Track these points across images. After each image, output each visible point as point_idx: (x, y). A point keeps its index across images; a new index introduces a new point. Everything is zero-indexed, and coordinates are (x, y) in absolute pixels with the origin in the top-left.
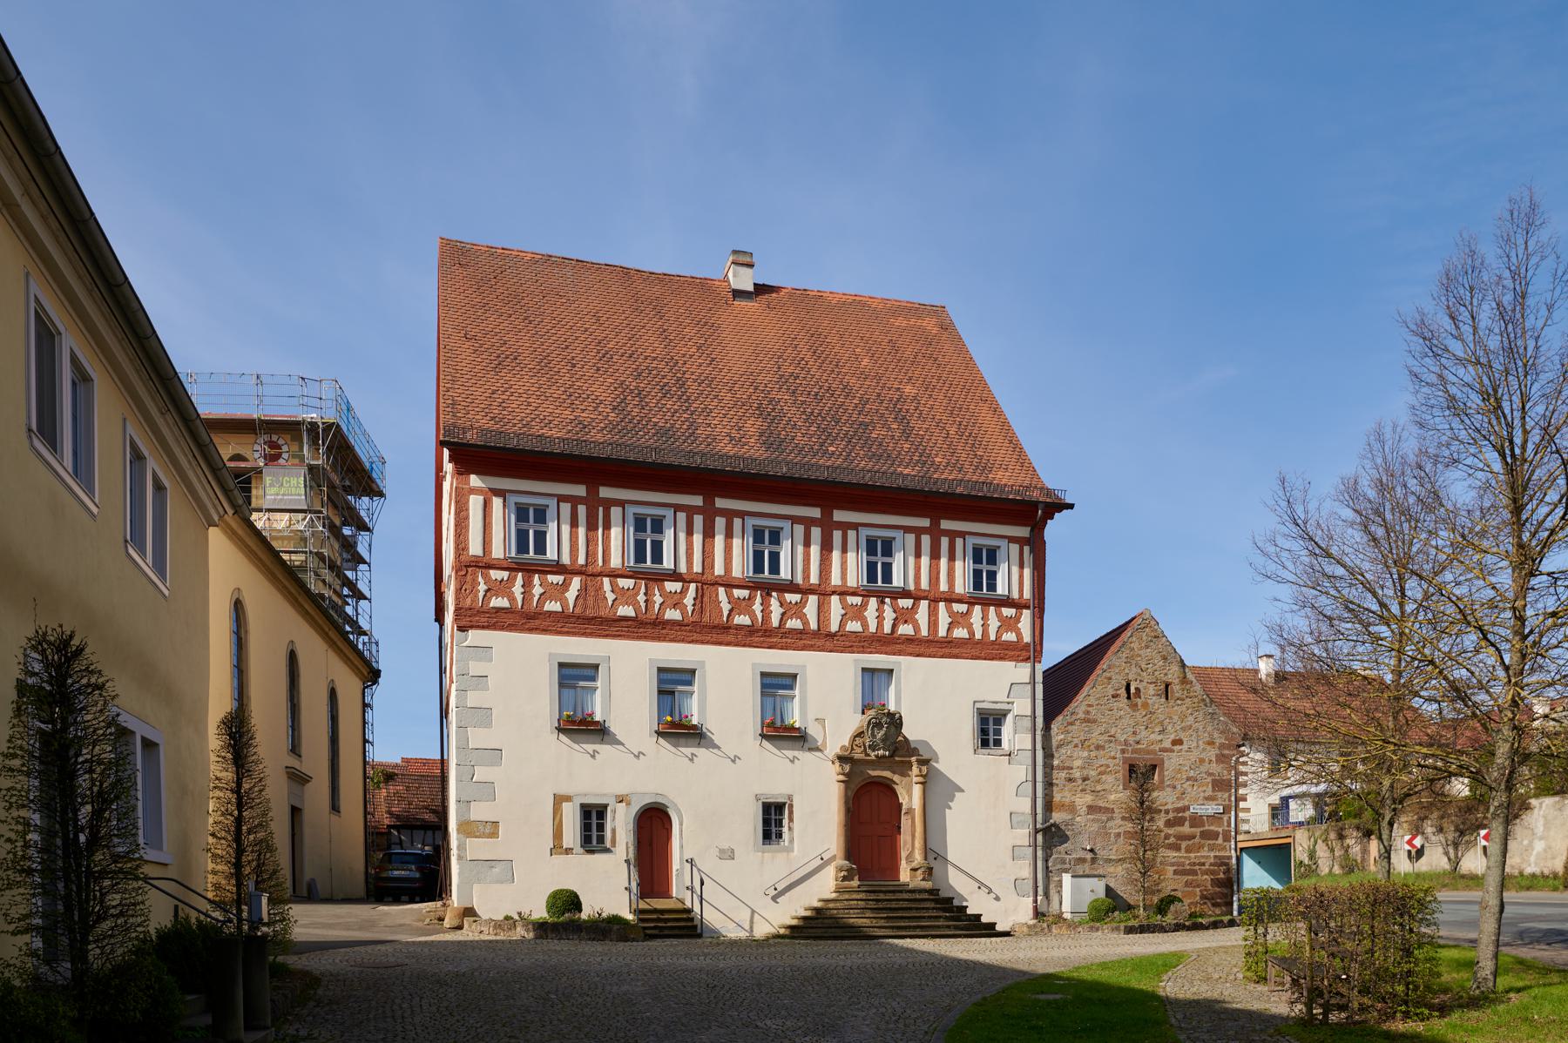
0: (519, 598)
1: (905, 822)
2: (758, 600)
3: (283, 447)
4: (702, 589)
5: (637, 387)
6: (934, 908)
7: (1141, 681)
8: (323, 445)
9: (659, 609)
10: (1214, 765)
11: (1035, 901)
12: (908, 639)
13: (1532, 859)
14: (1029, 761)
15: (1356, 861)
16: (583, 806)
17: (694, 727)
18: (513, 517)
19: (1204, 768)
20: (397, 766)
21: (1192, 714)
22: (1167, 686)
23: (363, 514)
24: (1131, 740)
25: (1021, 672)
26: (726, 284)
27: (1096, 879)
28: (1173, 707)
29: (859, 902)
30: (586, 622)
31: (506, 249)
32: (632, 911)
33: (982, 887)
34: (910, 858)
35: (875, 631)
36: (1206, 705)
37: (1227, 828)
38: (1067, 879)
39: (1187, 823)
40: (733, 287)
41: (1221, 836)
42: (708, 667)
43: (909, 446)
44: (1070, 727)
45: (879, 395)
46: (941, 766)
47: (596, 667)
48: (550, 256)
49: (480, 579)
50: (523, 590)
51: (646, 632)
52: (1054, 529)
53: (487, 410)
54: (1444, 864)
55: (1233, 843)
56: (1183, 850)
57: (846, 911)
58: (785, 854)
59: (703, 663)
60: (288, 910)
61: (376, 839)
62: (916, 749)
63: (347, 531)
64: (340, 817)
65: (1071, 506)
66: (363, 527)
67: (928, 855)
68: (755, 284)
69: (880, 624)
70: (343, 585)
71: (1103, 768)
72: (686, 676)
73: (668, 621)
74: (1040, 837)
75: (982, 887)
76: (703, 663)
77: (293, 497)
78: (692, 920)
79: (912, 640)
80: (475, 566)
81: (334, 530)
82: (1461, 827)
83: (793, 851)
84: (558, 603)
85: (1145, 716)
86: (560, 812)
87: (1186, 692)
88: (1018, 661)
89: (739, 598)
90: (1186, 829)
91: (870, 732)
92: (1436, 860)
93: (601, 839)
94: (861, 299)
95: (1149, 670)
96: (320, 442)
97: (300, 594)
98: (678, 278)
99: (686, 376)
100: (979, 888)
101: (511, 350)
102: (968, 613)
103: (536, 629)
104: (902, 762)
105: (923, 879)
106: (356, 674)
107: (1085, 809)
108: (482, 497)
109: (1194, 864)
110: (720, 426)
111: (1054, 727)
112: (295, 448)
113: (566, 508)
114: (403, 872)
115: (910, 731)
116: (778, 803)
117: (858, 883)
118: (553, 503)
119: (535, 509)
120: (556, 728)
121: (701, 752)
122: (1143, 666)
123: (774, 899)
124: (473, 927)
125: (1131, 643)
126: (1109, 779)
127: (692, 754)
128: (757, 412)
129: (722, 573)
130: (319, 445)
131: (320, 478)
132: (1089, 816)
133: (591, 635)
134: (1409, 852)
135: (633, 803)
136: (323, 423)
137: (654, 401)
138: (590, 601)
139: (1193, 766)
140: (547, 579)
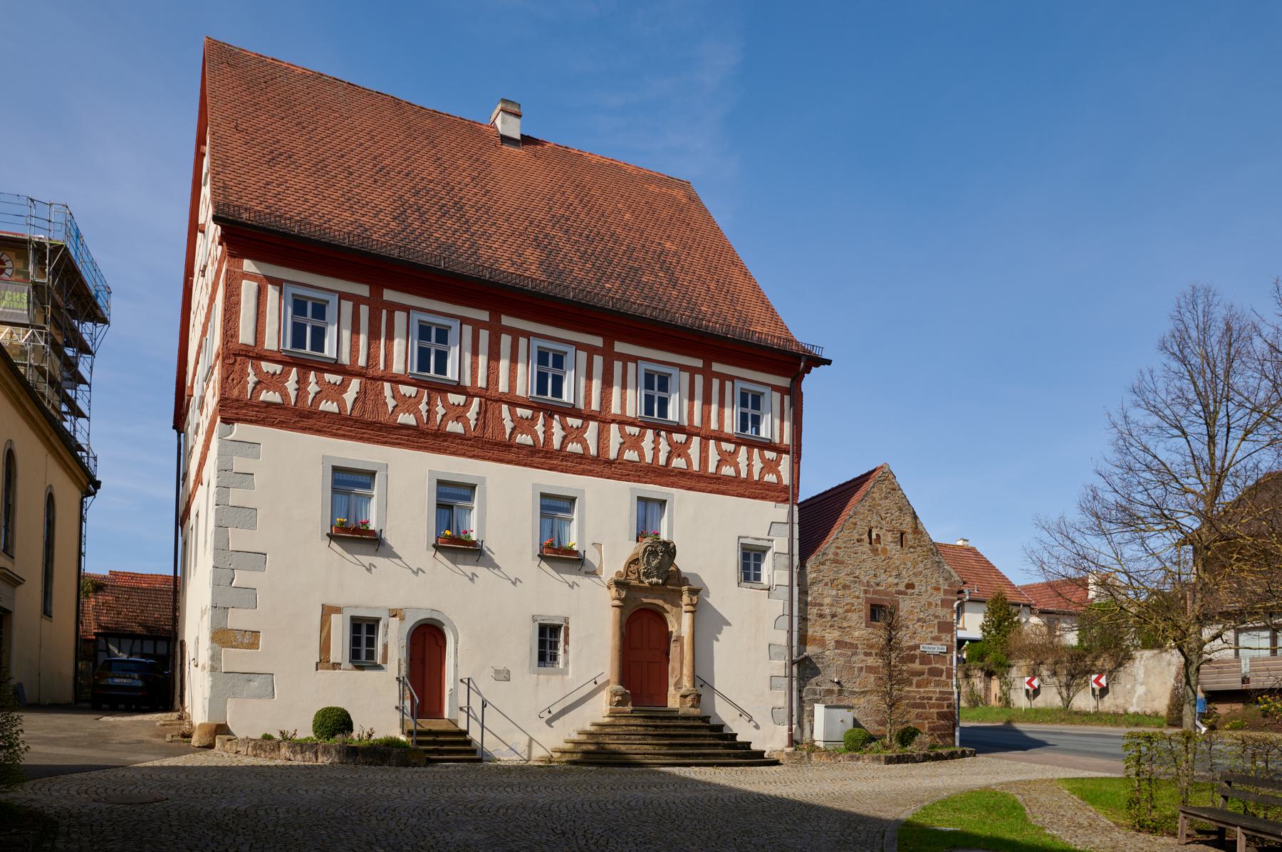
0: (293, 395)
1: (674, 650)
2: (541, 421)
3: (6, 263)
4: (486, 405)
5: (416, 203)
6: (711, 736)
7: (881, 528)
8: (50, 265)
9: (442, 420)
10: (940, 608)
11: (791, 730)
12: (680, 472)
13: (1134, 700)
14: (787, 596)
15: (980, 696)
16: (353, 619)
17: (474, 543)
18: (290, 310)
19: (931, 611)
20: (105, 577)
21: (922, 562)
22: (902, 534)
23: (86, 337)
24: (873, 581)
25: (780, 512)
26: (494, 130)
27: (846, 710)
28: (907, 554)
29: (639, 728)
30: (362, 426)
31: (276, 60)
32: (405, 732)
33: (743, 716)
34: (678, 685)
35: (651, 462)
36: (933, 554)
37: (948, 666)
38: (819, 710)
39: (917, 661)
40: (501, 133)
41: (944, 673)
42: (488, 483)
43: (677, 294)
44: (821, 567)
45: (643, 246)
46: (711, 600)
47: (373, 474)
48: (322, 75)
49: (250, 370)
50: (297, 387)
51: (426, 442)
52: (812, 382)
53: (262, 199)
54: (1057, 702)
55: (954, 680)
56: (914, 685)
57: (627, 737)
58: (560, 677)
59: (483, 479)
60: (17, 733)
61: (86, 649)
62: (685, 578)
63: (69, 352)
64: (51, 621)
65: (828, 362)
66: (85, 349)
67: (696, 683)
68: (521, 135)
69: (655, 456)
70: (63, 401)
71: (849, 607)
72: (467, 490)
73: (450, 434)
74: (795, 668)
75: (743, 716)
76: (483, 479)
77: (14, 311)
78: (469, 742)
79: (684, 473)
80: (245, 356)
81: (57, 349)
82: (1073, 671)
83: (567, 674)
84: (335, 403)
85: (884, 560)
86: (328, 624)
87: (917, 541)
88: (777, 502)
89: (522, 417)
90: (916, 666)
91: (645, 559)
92: (1051, 697)
93: (371, 655)
94: (617, 163)
95: (888, 519)
96: (47, 261)
97: (22, 393)
98: (448, 117)
99: (463, 201)
100: (741, 715)
101: (285, 149)
102: (736, 452)
103: (310, 429)
104: (673, 590)
105: (692, 707)
106: (75, 484)
107: (833, 643)
108: (256, 284)
109: (923, 698)
110: (500, 250)
111: (809, 565)
112: (20, 265)
113: (347, 306)
114: (125, 680)
115: (684, 563)
116: (554, 625)
117: (632, 708)
118: (333, 300)
119: (313, 303)
120: (328, 535)
121: (481, 571)
122: (883, 515)
123: (549, 722)
124: (228, 746)
125: (873, 493)
126: (854, 617)
127: (473, 574)
128: (534, 243)
129: (506, 390)
130: (46, 265)
131: (44, 297)
132: (836, 651)
133: (369, 440)
134: (1027, 691)
135: (407, 618)
136: (51, 244)
137: (434, 218)
138: (370, 406)
139: (922, 609)
140: (324, 377)
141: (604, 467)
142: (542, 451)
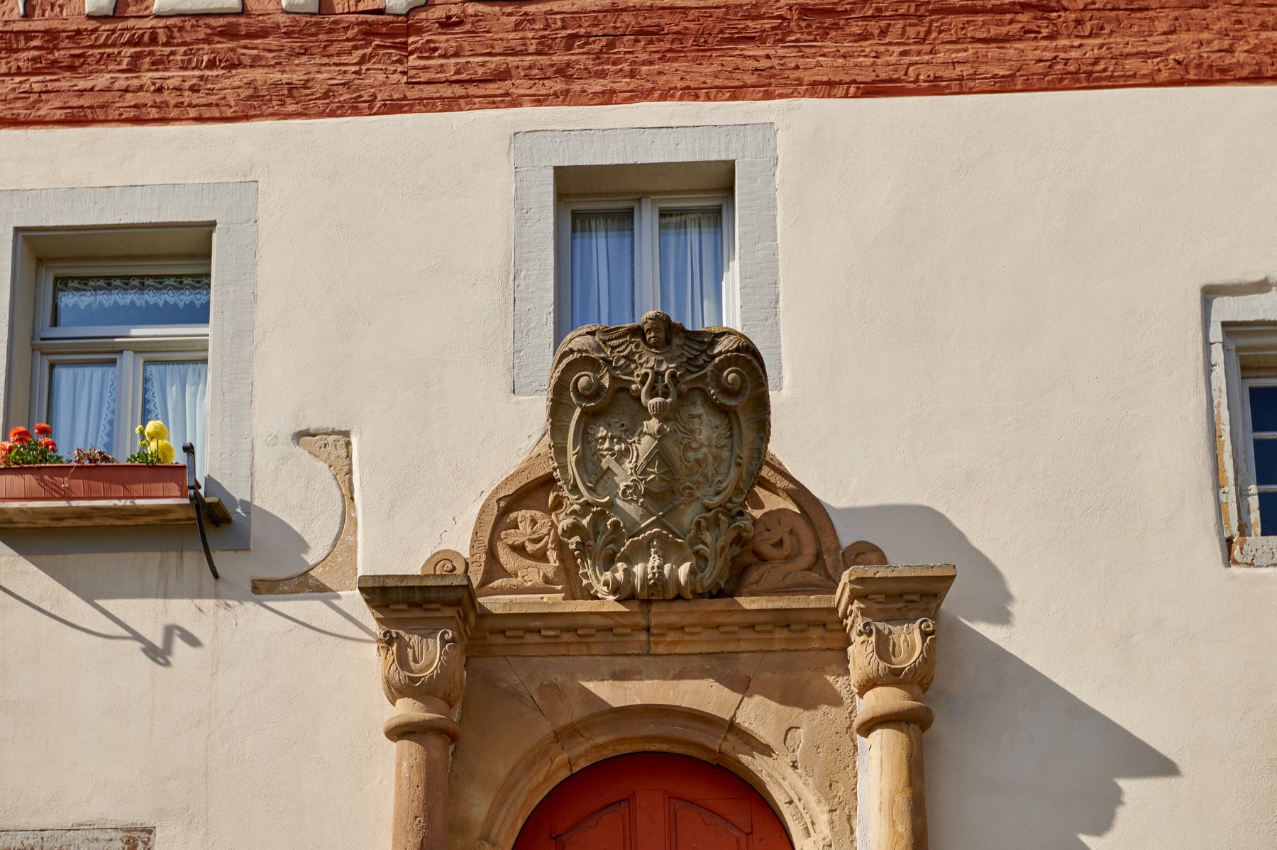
104: (783, 620)
141: (362, 61)
142: (28, 35)
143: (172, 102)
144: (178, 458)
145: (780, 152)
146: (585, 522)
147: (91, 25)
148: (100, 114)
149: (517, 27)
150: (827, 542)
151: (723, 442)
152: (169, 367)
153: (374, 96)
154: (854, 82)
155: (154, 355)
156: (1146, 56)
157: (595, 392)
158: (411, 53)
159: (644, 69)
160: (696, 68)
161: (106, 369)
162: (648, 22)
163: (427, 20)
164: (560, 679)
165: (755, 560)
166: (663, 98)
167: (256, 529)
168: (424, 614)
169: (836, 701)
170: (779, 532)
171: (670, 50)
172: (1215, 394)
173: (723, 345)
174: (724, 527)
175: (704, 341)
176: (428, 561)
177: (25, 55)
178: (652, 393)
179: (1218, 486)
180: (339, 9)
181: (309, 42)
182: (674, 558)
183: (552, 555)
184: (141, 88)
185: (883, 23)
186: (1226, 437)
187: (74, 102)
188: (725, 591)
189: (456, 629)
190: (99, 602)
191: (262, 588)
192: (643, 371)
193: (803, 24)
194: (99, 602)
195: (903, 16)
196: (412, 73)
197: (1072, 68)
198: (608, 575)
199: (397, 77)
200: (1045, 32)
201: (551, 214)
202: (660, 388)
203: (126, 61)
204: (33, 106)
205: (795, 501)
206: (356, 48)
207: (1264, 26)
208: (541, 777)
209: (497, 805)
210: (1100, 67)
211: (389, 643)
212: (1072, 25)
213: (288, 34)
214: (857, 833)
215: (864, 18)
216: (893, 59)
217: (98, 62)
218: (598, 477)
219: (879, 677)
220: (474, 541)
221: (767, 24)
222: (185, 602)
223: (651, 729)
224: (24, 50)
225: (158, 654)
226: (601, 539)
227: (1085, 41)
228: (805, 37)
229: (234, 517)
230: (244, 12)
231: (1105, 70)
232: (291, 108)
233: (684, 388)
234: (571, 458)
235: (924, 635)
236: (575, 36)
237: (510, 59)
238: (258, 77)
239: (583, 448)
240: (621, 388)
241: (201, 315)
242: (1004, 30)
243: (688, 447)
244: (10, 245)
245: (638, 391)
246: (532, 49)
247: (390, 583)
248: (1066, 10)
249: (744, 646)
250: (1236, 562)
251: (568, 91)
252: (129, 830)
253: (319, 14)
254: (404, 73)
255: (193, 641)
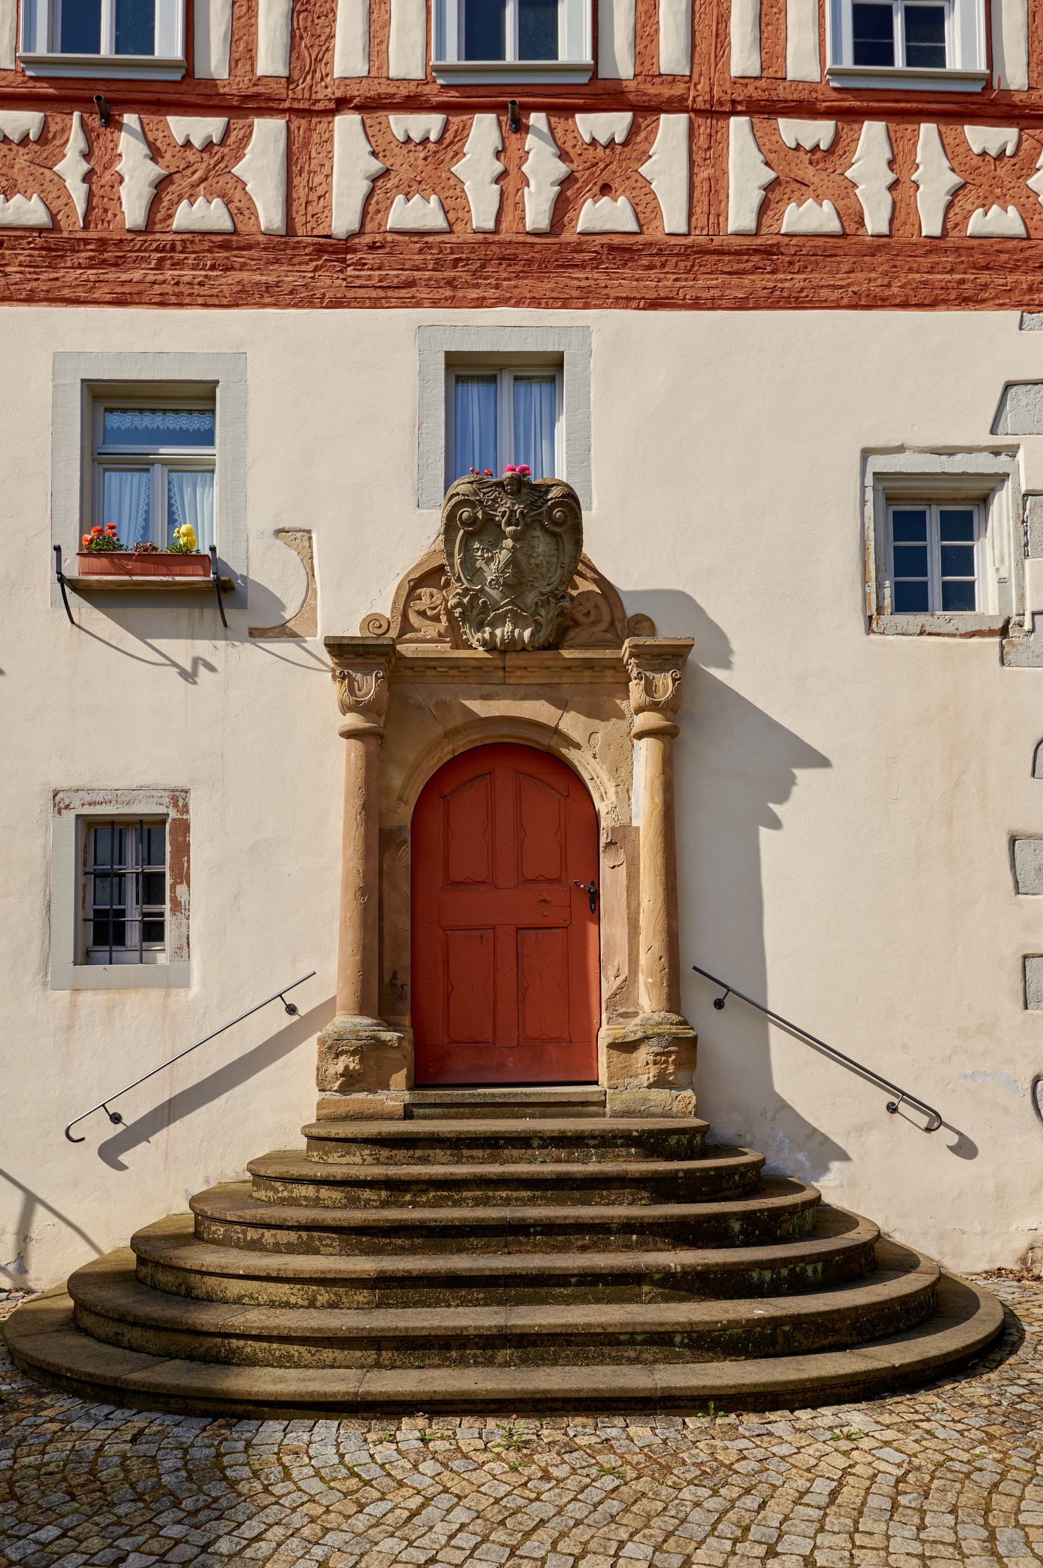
104: (589, 664)
141: (316, 269)
142: (86, 241)
143: (186, 293)
144: (208, 552)
145: (593, 347)
146: (465, 600)
147: (130, 236)
148: (137, 299)
149: (420, 251)
150: (618, 614)
151: (553, 553)
152: (185, 474)
153: (324, 295)
154: (643, 298)
155: (174, 466)
156: (834, 287)
157: (473, 521)
158: (349, 265)
159: (505, 283)
160: (539, 284)
161: (141, 474)
162: (508, 252)
163: (360, 244)
164: (448, 698)
165: (572, 623)
166: (517, 305)
167: (251, 595)
168: (364, 661)
169: (621, 716)
170: (589, 606)
171: (522, 272)
172: (866, 520)
173: (554, 493)
174: (553, 606)
175: (543, 489)
176: (364, 620)
177: (83, 255)
178: (509, 523)
179: (865, 581)
180: (300, 232)
181: (280, 255)
182: (521, 624)
183: (443, 618)
184: (164, 282)
185: (663, 259)
186: (872, 550)
187: (119, 290)
188: (553, 646)
189: (384, 671)
190: (149, 641)
191: (256, 634)
192: (503, 509)
193: (611, 257)
194: (149, 641)
195: (676, 255)
196: (350, 280)
197: (785, 294)
198: (479, 635)
199: (339, 282)
200: (769, 269)
201: (443, 385)
202: (513, 520)
203: (154, 262)
204: (90, 290)
205: (598, 586)
206: (311, 260)
207: (911, 270)
208: (435, 760)
209: (410, 777)
210: (804, 294)
211: (343, 678)
212: (786, 265)
213: (265, 249)
214: (633, 800)
215: (651, 255)
216: (669, 283)
217: (134, 262)
218: (473, 573)
219: (646, 706)
220: (393, 608)
221: (587, 256)
222: (206, 642)
223: (505, 730)
224: (83, 251)
225: (189, 676)
226: (476, 611)
227: (795, 276)
228: (612, 266)
229: (236, 586)
230: (235, 232)
231: (807, 296)
232: (268, 300)
233: (529, 520)
234: (457, 561)
235: (674, 680)
236: (460, 259)
237: (415, 273)
238: (245, 277)
239: (464, 555)
240: (489, 519)
241: (207, 438)
242: (742, 266)
243: (531, 556)
244: (79, 392)
245: (500, 521)
246: (430, 267)
247: (345, 642)
248: (783, 254)
249: (565, 680)
250: (873, 632)
251: (454, 297)
252: (173, 791)
253: (287, 236)
254: (344, 279)
255: (212, 668)
